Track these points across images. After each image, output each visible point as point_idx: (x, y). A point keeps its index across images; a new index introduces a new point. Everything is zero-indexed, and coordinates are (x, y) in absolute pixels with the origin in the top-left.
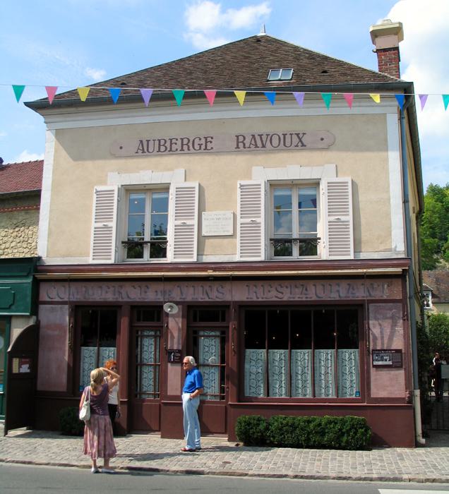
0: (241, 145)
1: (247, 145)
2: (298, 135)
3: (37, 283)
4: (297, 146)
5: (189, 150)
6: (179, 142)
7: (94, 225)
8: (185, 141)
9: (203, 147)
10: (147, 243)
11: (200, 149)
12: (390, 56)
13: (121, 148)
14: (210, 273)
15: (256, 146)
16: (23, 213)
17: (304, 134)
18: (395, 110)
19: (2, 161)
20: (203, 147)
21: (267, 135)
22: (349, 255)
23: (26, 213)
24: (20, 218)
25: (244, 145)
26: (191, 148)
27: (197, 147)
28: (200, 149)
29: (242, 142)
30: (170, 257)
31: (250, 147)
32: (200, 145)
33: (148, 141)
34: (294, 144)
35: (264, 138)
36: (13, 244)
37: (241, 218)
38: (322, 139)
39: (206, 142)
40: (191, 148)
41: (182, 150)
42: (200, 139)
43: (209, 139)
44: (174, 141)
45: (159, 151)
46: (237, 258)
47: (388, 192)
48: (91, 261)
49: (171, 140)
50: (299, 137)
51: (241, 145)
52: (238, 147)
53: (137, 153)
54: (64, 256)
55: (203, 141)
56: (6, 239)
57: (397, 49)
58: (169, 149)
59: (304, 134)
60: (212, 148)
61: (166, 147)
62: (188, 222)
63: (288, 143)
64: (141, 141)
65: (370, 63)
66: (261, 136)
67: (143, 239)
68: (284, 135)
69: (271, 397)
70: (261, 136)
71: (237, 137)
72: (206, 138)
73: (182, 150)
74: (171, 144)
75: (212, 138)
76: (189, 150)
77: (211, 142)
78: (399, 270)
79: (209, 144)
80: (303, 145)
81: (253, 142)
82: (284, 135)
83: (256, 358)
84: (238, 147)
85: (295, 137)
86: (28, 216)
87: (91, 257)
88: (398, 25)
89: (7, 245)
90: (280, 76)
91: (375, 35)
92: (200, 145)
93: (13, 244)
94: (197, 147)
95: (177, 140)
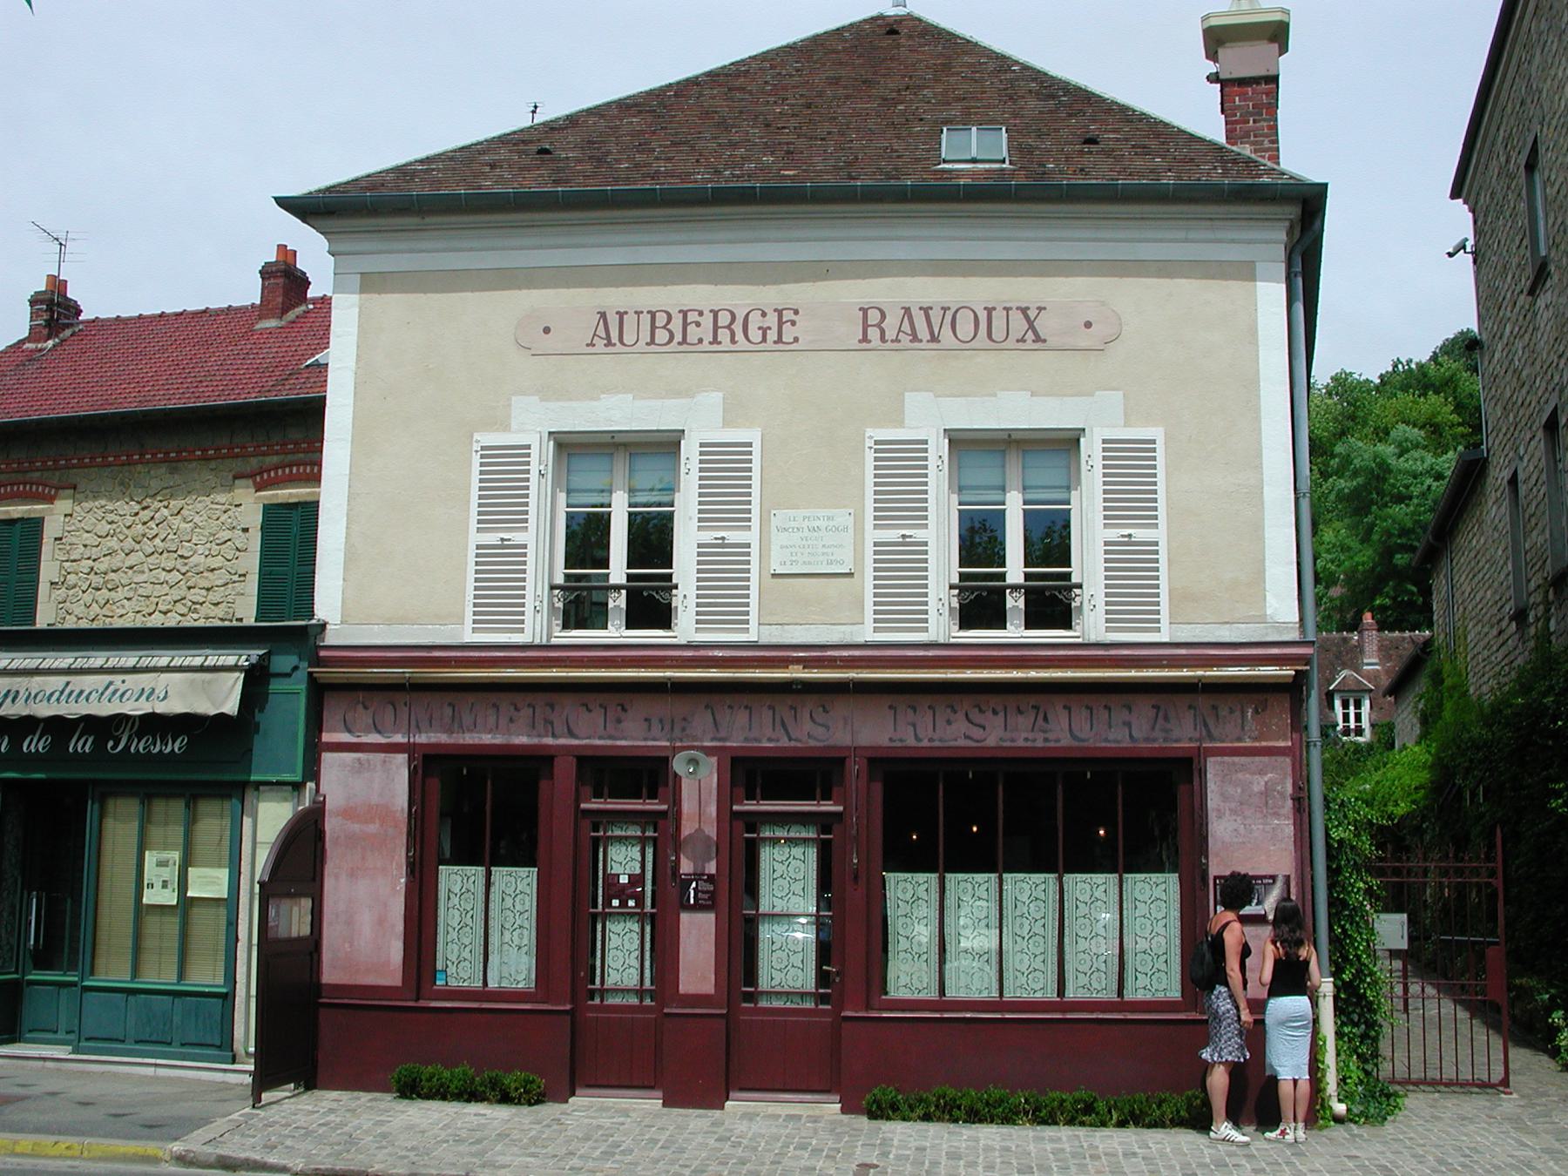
0: (873, 333)
1: (890, 335)
2: (1024, 311)
3: (319, 692)
4: (1022, 340)
5: (733, 341)
6: (707, 320)
7: (475, 538)
8: (724, 319)
9: (772, 335)
10: (617, 588)
11: (764, 339)
12: (1251, 98)
13: (547, 330)
14: (796, 673)
15: (915, 338)
16: (163, 470)
17: (1040, 309)
18: (1280, 251)
19: (79, 312)
20: (772, 335)
21: (945, 309)
22: (1158, 630)
23: (173, 471)
24: (153, 483)
25: (883, 332)
26: (739, 336)
27: (756, 335)
28: (764, 339)
29: (878, 326)
30: (686, 628)
31: (897, 340)
32: (764, 330)
33: (621, 315)
34: (1014, 335)
35: (935, 316)
36: (133, 559)
37: (479, 530)
38: (1088, 325)
39: (781, 324)
40: (739, 336)
41: (715, 341)
42: (764, 314)
43: (788, 315)
44: (692, 317)
45: (652, 342)
46: (867, 633)
47: (1259, 468)
48: (469, 635)
49: (685, 314)
50: (1035, 333)
51: (873, 333)
52: (865, 339)
53: (592, 345)
54: (389, 622)
55: (772, 320)
56: (113, 543)
57: (1274, 79)
58: (678, 337)
59: (1040, 309)
60: (796, 340)
61: (673, 333)
62: (734, 537)
63: (998, 333)
64: (603, 315)
65: (1203, 116)
66: (926, 311)
67: (1002, 577)
68: (990, 311)
69: (1070, 994)
70: (926, 311)
71: (865, 311)
72: (780, 313)
73: (715, 341)
74: (685, 325)
75: (796, 312)
76: (733, 341)
77: (793, 323)
78: (1288, 672)
79: (787, 327)
80: (1038, 339)
81: (906, 327)
82: (990, 311)
83: (909, 895)
84: (865, 339)
85: (1017, 317)
86: (177, 479)
87: (469, 625)
88: (1277, 17)
89: (116, 561)
90: (973, 149)
91: (1216, 39)
92: (764, 330)
93: (133, 559)
94: (756, 335)
95: (701, 314)
